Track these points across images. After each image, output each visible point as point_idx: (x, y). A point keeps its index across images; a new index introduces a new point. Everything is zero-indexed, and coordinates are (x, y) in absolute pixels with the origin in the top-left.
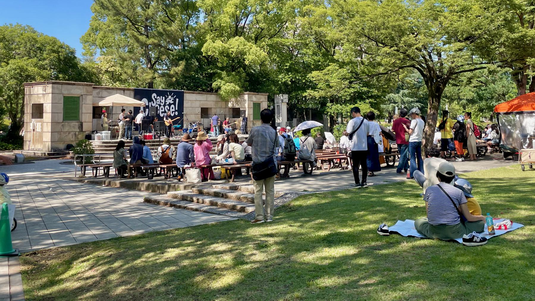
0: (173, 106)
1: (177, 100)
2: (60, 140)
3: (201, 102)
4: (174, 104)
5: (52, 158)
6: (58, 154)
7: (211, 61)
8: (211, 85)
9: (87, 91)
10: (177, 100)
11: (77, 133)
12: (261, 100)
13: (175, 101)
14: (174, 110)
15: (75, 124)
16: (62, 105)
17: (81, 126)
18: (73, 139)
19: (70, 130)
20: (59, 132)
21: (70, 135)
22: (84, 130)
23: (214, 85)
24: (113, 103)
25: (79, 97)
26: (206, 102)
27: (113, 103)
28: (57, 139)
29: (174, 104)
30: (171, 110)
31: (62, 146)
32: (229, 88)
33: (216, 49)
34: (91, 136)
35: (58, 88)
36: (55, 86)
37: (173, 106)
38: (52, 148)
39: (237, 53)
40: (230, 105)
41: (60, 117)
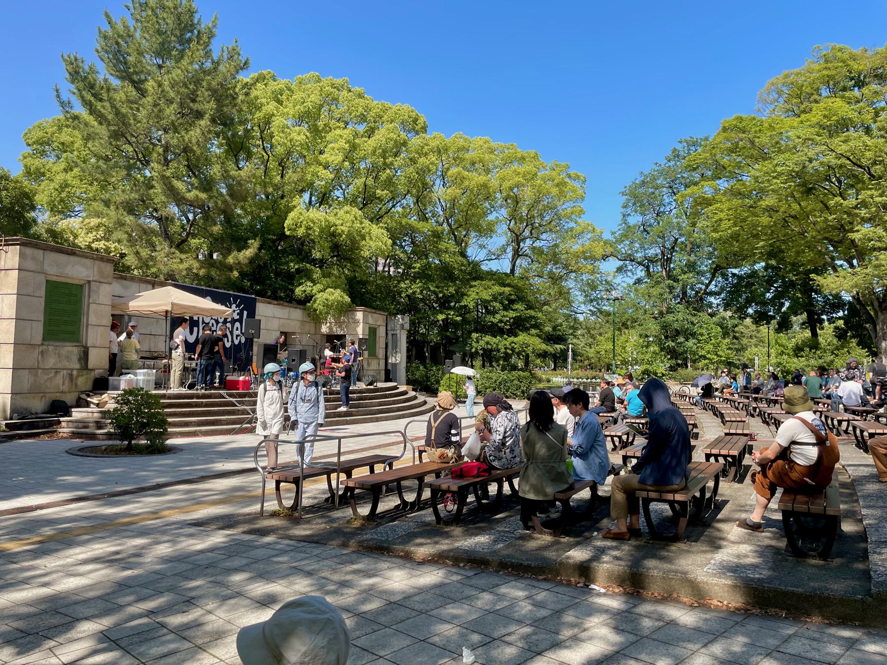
0: (237, 324)
1: (245, 313)
2: (36, 391)
3: (282, 321)
4: (240, 320)
5: (21, 437)
6: (32, 426)
7: (300, 249)
8: (293, 291)
9: (101, 273)
10: (245, 313)
11: (75, 373)
12: (379, 323)
13: (241, 314)
14: (238, 332)
15: (71, 350)
16: (42, 300)
17: (84, 356)
18: (65, 388)
19: (59, 366)
20: (33, 370)
21: (59, 379)
22: (90, 366)
23: (298, 291)
24: (173, 304)
25: (81, 286)
26: (289, 321)
27: (173, 304)
28: (26, 386)
29: (240, 320)
30: (236, 333)
31: (38, 405)
32: (331, 298)
33: (314, 223)
34: (108, 380)
35: (34, 258)
36: (29, 251)
37: (237, 324)
38: (13, 411)
39: (349, 234)
40: (324, 329)
41: (37, 331)
